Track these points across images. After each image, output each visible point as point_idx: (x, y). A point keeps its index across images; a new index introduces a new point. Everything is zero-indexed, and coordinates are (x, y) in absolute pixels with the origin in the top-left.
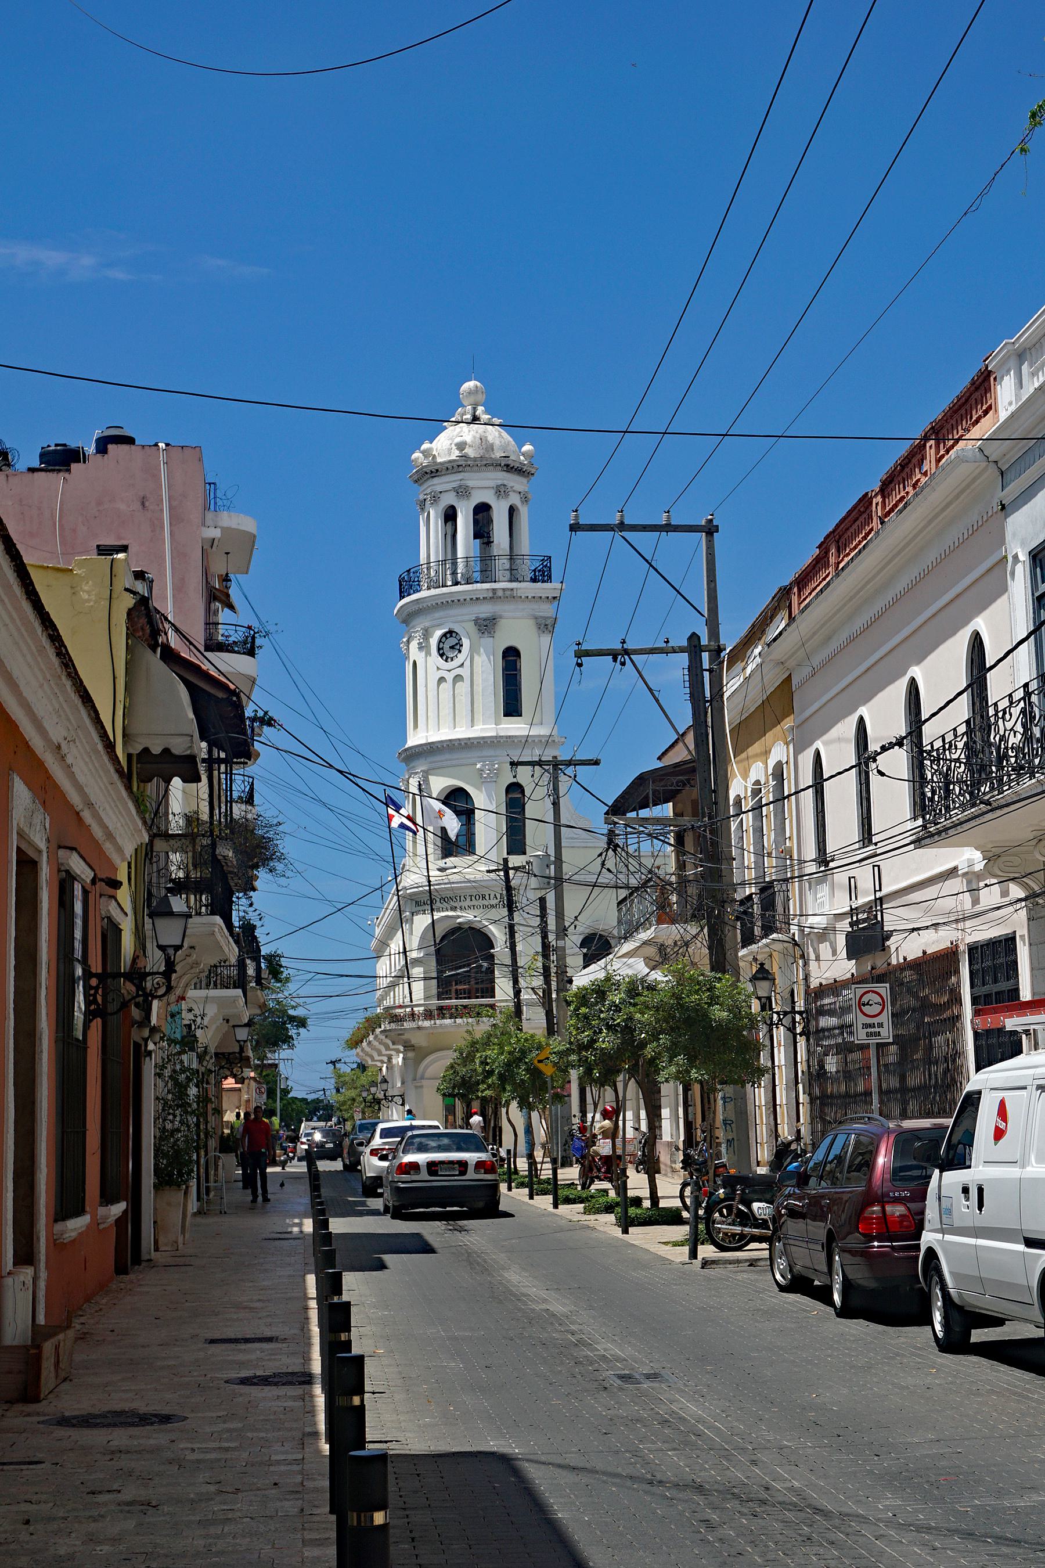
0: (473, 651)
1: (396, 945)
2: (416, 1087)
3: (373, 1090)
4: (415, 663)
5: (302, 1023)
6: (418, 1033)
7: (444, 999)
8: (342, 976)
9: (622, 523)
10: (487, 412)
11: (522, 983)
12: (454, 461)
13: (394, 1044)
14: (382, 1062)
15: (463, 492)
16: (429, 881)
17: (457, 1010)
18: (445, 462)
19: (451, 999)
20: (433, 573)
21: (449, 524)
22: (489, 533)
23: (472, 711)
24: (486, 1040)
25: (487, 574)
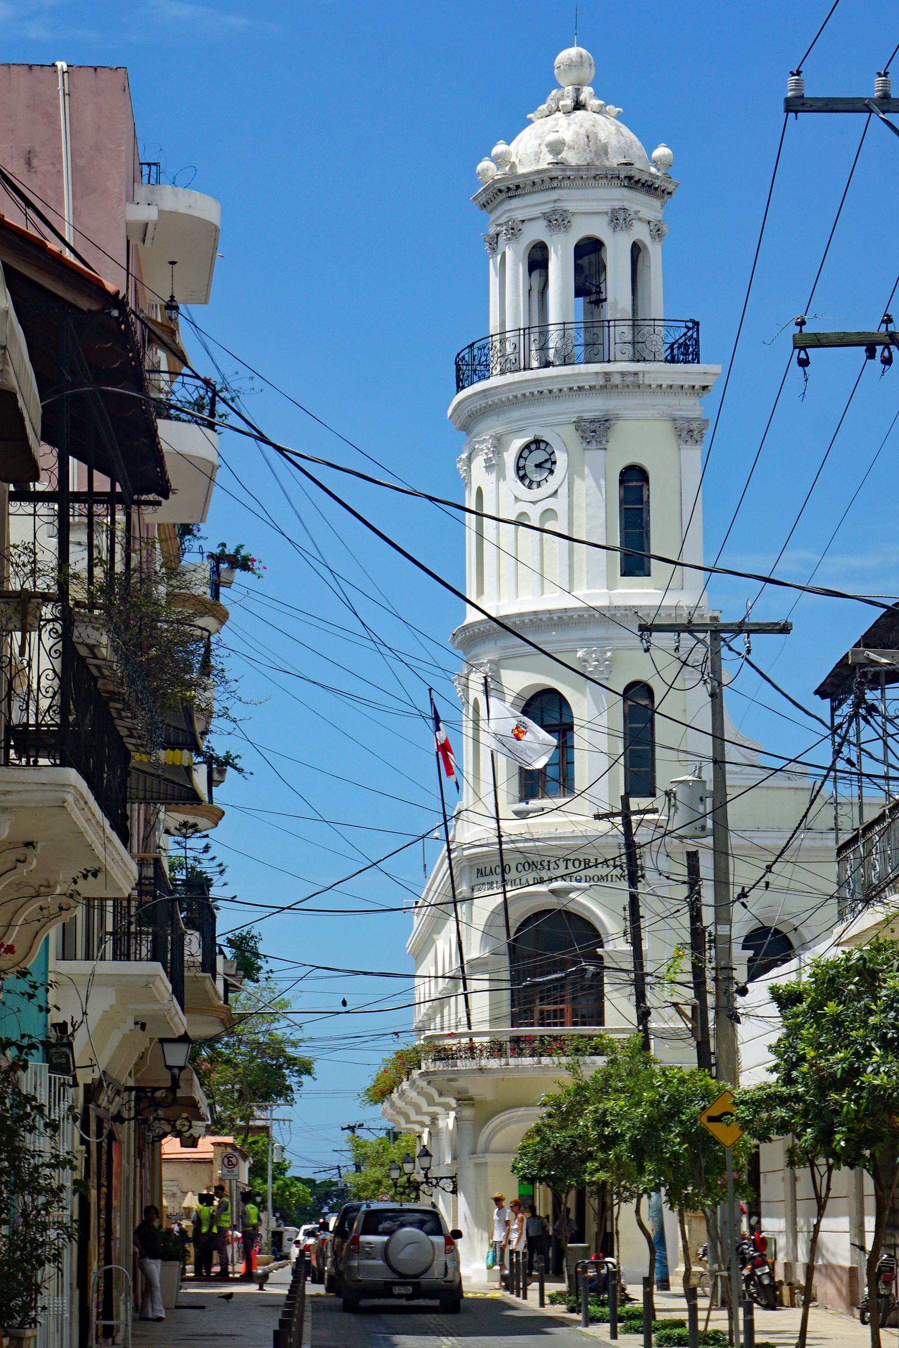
0: (573, 471)
1: (445, 944)
2: (477, 1165)
3: (408, 1167)
4: (480, 492)
5: (306, 1069)
6: (481, 1079)
7: (521, 1025)
8: (357, 973)
9: (885, 96)
10: (597, 95)
11: (651, 999)
12: (544, 171)
13: (441, 1094)
14: (423, 1125)
15: (558, 220)
16: (500, 836)
17: (542, 1041)
18: (531, 173)
19: (532, 1025)
20: (509, 349)
21: (536, 273)
22: (599, 287)
23: (571, 567)
24: (601, 1083)
25: (594, 349)
